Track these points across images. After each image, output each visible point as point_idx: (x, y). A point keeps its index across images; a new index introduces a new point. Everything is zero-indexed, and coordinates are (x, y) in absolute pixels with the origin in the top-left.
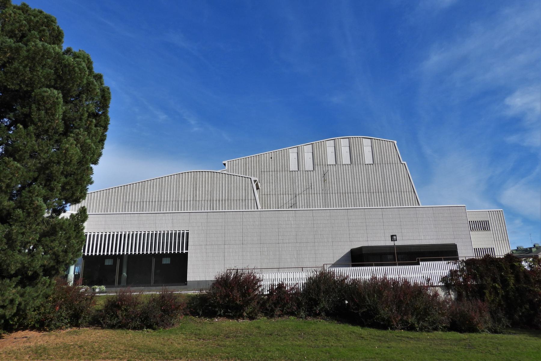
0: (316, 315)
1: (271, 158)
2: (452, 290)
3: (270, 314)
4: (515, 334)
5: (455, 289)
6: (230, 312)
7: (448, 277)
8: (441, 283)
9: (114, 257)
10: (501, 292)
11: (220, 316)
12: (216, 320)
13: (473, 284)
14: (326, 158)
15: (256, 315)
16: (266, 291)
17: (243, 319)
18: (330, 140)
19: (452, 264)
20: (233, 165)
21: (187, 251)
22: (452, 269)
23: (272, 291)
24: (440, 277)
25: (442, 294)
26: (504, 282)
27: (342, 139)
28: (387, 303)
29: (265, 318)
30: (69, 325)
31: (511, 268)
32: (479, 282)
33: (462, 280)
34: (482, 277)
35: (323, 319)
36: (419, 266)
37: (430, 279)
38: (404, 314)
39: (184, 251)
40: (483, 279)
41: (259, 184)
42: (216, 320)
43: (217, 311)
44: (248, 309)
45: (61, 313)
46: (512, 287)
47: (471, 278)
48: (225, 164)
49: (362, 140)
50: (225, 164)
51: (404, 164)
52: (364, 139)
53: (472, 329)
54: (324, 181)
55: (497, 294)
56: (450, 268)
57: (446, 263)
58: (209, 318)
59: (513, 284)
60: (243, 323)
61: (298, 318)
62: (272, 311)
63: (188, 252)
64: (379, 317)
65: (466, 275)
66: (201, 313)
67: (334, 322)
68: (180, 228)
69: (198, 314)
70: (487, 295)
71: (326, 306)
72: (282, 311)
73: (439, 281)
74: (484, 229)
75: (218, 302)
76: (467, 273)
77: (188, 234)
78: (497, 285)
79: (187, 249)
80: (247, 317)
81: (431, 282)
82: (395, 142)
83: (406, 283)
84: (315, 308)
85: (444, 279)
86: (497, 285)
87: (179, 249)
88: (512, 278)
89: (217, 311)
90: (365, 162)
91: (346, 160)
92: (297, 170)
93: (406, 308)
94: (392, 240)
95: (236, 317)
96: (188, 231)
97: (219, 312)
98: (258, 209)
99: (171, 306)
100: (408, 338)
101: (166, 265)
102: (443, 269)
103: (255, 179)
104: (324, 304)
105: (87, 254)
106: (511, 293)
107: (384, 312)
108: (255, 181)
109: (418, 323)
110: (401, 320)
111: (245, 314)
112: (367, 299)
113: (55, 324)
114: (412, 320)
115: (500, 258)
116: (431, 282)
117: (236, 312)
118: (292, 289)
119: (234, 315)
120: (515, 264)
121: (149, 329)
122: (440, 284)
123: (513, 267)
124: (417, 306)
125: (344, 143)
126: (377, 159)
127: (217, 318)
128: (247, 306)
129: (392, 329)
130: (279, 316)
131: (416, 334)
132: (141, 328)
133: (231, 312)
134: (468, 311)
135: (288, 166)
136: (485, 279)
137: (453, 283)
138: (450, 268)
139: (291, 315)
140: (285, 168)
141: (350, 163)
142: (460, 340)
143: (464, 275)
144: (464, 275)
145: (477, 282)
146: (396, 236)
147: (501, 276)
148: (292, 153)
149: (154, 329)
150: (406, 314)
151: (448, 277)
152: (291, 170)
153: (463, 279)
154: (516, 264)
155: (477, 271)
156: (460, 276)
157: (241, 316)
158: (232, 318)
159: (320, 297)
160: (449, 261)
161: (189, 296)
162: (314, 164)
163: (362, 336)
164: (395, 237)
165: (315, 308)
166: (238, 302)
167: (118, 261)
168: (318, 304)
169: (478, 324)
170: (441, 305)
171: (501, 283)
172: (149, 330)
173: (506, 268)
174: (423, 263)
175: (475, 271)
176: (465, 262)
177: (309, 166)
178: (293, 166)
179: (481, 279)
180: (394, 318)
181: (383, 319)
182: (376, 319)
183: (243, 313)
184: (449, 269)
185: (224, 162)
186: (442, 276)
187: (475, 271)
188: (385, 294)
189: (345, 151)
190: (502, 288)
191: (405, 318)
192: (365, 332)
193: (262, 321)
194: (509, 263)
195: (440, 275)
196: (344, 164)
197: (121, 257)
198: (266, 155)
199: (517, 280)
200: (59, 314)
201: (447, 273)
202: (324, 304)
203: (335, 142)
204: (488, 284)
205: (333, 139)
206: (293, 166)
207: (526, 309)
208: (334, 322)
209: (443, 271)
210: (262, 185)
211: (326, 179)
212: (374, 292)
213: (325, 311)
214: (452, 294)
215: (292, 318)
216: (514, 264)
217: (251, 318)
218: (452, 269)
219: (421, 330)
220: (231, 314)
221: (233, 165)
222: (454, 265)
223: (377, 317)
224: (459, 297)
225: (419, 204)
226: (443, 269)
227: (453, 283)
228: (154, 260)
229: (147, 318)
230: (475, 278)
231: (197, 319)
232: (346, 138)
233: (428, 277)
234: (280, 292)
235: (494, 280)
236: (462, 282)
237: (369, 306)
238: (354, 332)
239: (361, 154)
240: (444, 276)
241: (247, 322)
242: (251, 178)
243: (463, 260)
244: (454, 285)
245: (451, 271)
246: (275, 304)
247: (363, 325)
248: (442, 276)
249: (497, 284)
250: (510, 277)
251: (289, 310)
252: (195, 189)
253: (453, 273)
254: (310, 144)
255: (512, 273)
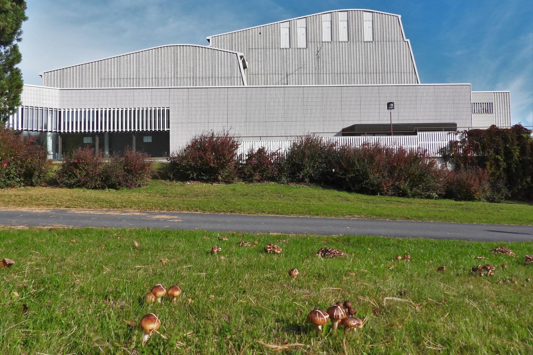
0: (301, 181)
1: (260, 33)
2: (450, 162)
3: (247, 178)
4: (514, 204)
5: (453, 161)
6: (204, 176)
7: (447, 149)
8: (438, 154)
9: (93, 135)
10: (503, 165)
11: (193, 179)
12: (189, 183)
13: (474, 156)
14: (321, 35)
15: (233, 179)
16: (245, 156)
17: (219, 183)
18: (327, 13)
19: (453, 134)
20: (218, 41)
21: (169, 129)
22: (453, 140)
23: (251, 156)
24: (438, 148)
25: (439, 165)
26: (508, 154)
27: (339, 13)
28: (378, 167)
29: (244, 183)
30: (22, 184)
31: (517, 140)
32: (480, 154)
33: (462, 152)
34: (484, 149)
35: (307, 185)
36: (416, 136)
37: (427, 150)
38: (396, 180)
39: (166, 129)
40: (484, 151)
41: (247, 63)
42: (189, 183)
43: (189, 175)
44: (224, 173)
45: (10, 171)
46: (515, 160)
47: (472, 150)
48: (209, 40)
49: (363, 13)
50: (209, 40)
51: (407, 42)
52: (364, 13)
53: (469, 197)
54: (317, 58)
55: (498, 167)
56: (451, 139)
57: (446, 133)
58: (181, 181)
59: (517, 156)
60: (216, 187)
61: (279, 183)
62: (251, 175)
63: (169, 130)
64: (368, 182)
65: (467, 146)
66: (172, 176)
67: (319, 188)
68: (160, 104)
69: (170, 178)
70: (488, 167)
71: (311, 171)
72: (262, 176)
73: (436, 152)
74: (487, 112)
75: (190, 165)
76: (468, 144)
77: (168, 111)
78: (499, 157)
79: (168, 127)
80: (222, 181)
81: (428, 153)
82: (400, 16)
83: (401, 151)
84: (298, 174)
85: (442, 150)
86: (499, 157)
87: (159, 127)
88: (518, 150)
89: (189, 175)
90: (364, 39)
91: (343, 36)
92: (288, 47)
93: (399, 174)
94: (388, 109)
95: (210, 181)
96: (169, 109)
97: (191, 175)
98: (244, 85)
99: (135, 165)
100: (399, 202)
101: (148, 143)
102: (442, 140)
103: (242, 54)
104: (308, 170)
105: (68, 132)
106: (514, 166)
107: (374, 177)
108: (241, 57)
109: (411, 190)
110: (392, 185)
111: (220, 178)
112: (357, 163)
113: (5, 182)
114: (404, 185)
115: (506, 129)
116: (428, 153)
117: (211, 176)
118: (274, 154)
119: (208, 179)
120: (523, 135)
121: (112, 189)
122: (438, 155)
123: (520, 138)
124: (411, 171)
125: (342, 16)
126: (378, 37)
127: (189, 181)
128: (222, 169)
129: (381, 194)
130: (259, 181)
131: (407, 199)
132: (103, 188)
133: (205, 176)
134: (467, 180)
135: (279, 43)
136: (487, 150)
137: (451, 155)
138: (451, 139)
139: (272, 181)
140: (276, 44)
141: (347, 40)
142: (456, 205)
143: (465, 146)
144: (465, 146)
145: (478, 154)
146: (393, 103)
147: (506, 148)
148: (284, 28)
149: (117, 189)
150: (399, 179)
151: (447, 149)
152: (282, 47)
153: (463, 151)
154: (525, 135)
155: (479, 142)
156: (461, 147)
157: (216, 180)
158: (206, 181)
159: (304, 163)
160: (450, 132)
161: (163, 163)
162: (308, 41)
163: (349, 199)
164: (392, 105)
165: (298, 174)
166: (212, 165)
167: (97, 139)
168: (301, 170)
169: (476, 192)
170: (438, 174)
171: (504, 156)
172: (111, 190)
173: (512, 140)
174: (420, 133)
175: (478, 143)
176: (467, 133)
177: (301, 42)
178: (284, 43)
179: (483, 150)
180: (386, 184)
181: (372, 185)
182: (365, 184)
183: (217, 176)
184: (449, 140)
185: (208, 38)
186: (440, 147)
187: (478, 143)
188: (377, 159)
189: (342, 26)
190: (504, 161)
191: (397, 183)
192: (352, 196)
193: (240, 186)
194: (517, 134)
195: (438, 146)
196: (340, 41)
197: (101, 135)
198: (255, 30)
199: (523, 152)
200: (7, 171)
201: (446, 144)
202: (308, 170)
203: (332, 15)
204: (490, 155)
205: (329, 13)
206: (284, 43)
207: (527, 182)
208: (319, 188)
209: (442, 142)
210: (249, 63)
211: (319, 56)
212: (365, 156)
213: (309, 177)
214: (449, 166)
215: (273, 183)
216: (522, 136)
217: (228, 182)
218: (453, 140)
219: (414, 196)
220: (204, 177)
221: (218, 41)
222: (455, 136)
223: (366, 183)
224: (457, 168)
225: (418, 83)
226: (442, 140)
227: (451, 155)
228: (134, 138)
229: (108, 178)
230: (476, 150)
231: (168, 182)
232: (345, 11)
233: (425, 148)
234: (260, 157)
235: (497, 152)
236: (461, 154)
237: (358, 171)
238: (339, 196)
239: (360, 31)
240: (442, 147)
241: (222, 186)
242: (236, 54)
243: (465, 131)
244: (453, 156)
245: (451, 142)
246: (254, 169)
247: (349, 190)
248: (440, 147)
249: (500, 156)
250: (515, 149)
251: (269, 175)
252: (176, 65)
253: (453, 144)
254: (303, 18)
255: (518, 145)
